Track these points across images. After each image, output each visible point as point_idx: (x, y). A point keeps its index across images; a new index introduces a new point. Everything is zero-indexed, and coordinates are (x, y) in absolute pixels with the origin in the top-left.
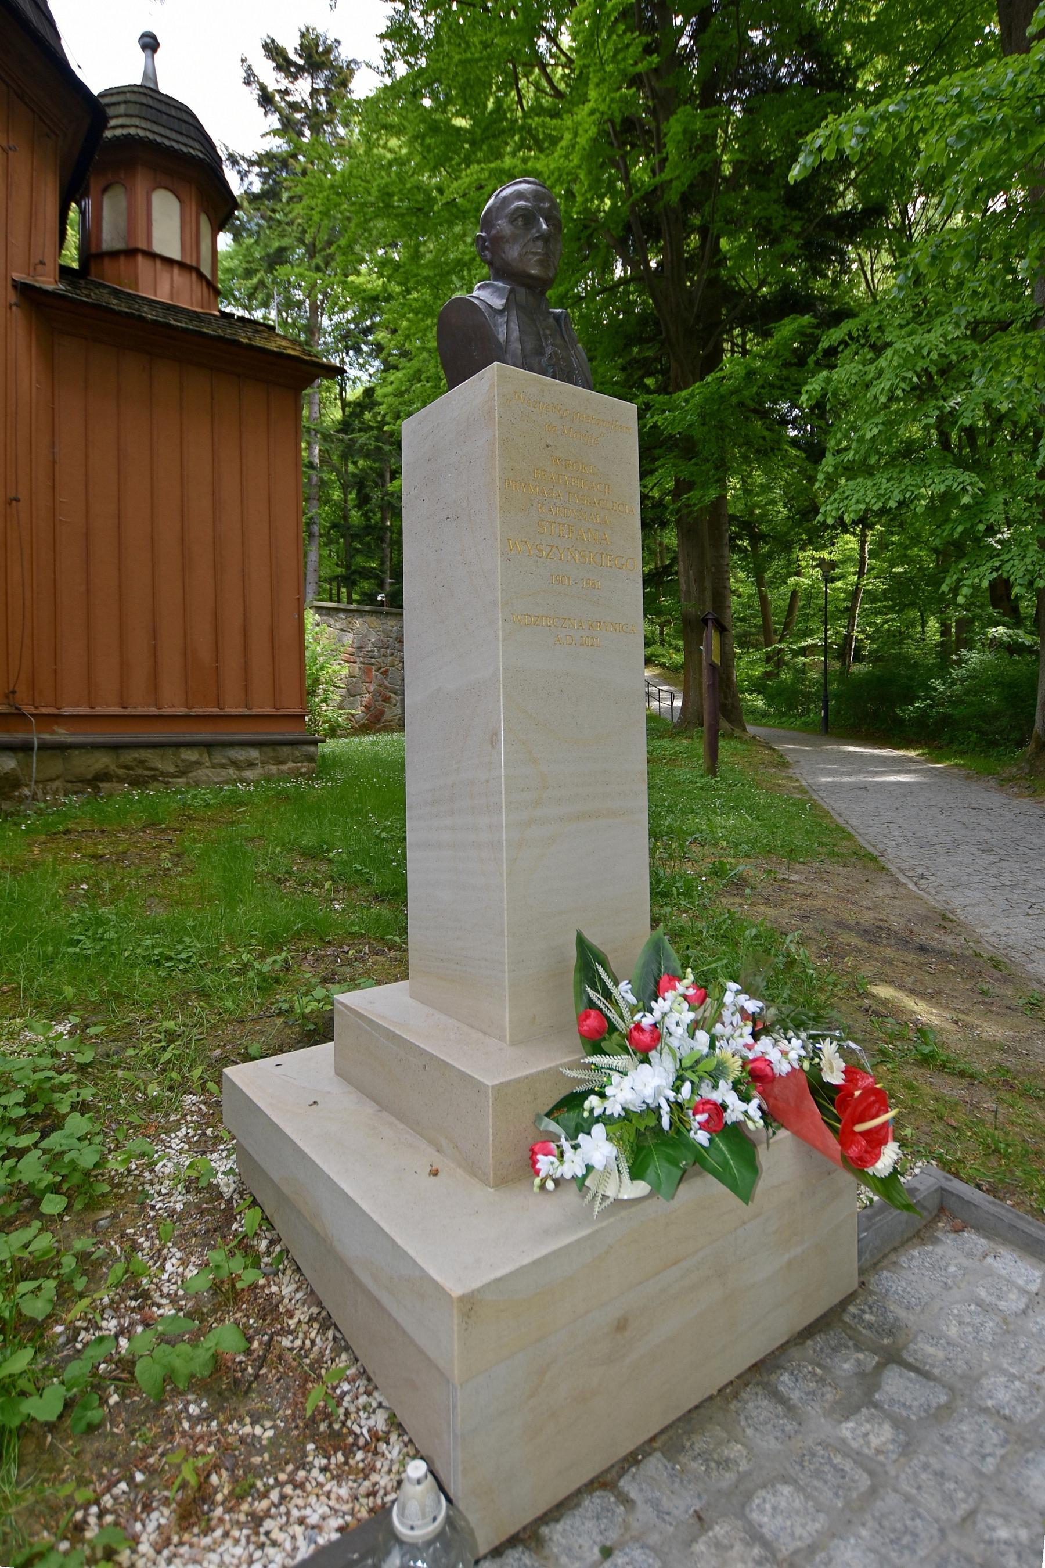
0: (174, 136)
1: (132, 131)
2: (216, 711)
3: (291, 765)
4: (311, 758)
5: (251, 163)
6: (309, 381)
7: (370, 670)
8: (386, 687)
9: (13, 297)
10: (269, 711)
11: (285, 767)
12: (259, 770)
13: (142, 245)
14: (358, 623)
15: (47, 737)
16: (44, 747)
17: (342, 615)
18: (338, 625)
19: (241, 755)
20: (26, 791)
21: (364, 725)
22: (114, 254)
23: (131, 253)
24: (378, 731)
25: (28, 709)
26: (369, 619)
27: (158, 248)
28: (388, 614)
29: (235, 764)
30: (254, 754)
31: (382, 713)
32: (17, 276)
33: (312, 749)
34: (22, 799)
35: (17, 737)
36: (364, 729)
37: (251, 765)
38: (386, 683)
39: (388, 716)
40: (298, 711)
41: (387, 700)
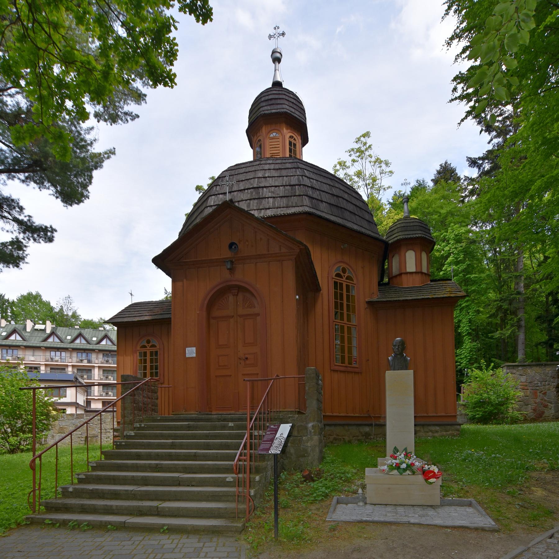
0: (411, 232)
1: (399, 238)
2: (425, 415)
3: (451, 432)
4: (458, 431)
5: (483, 159)
6: (457, 302)
7: (536, 393)
8: (545, 400)
9: (366, 306)
10: (443, 414)
11: (448, 433)
12: (439, 434)
13: (403, 271)
14: (529, 371)
15: (378, 423)
16: (376, 425)
17: (520, 368)
18: (518, 373)
19: (433, 428)
20: (372, 437)
21: (533, 418)
22: (396, 276)
23: (401, 274)
24: (542, 421)
25: (372, 415)
26: (535, 368)
27: (408, 270)
28: (545, 365)
29: (431, 431)
30: (437, 428)
31: (543, 413)
32: (367, 300)
33: (458, 427)
34: (371, 439)
35: (370, 422)
36: (533, 420)
37: (437, 432)
38: (546, 398)
39: (546, 414)
40: (454, 414)
41: (546, 406)
